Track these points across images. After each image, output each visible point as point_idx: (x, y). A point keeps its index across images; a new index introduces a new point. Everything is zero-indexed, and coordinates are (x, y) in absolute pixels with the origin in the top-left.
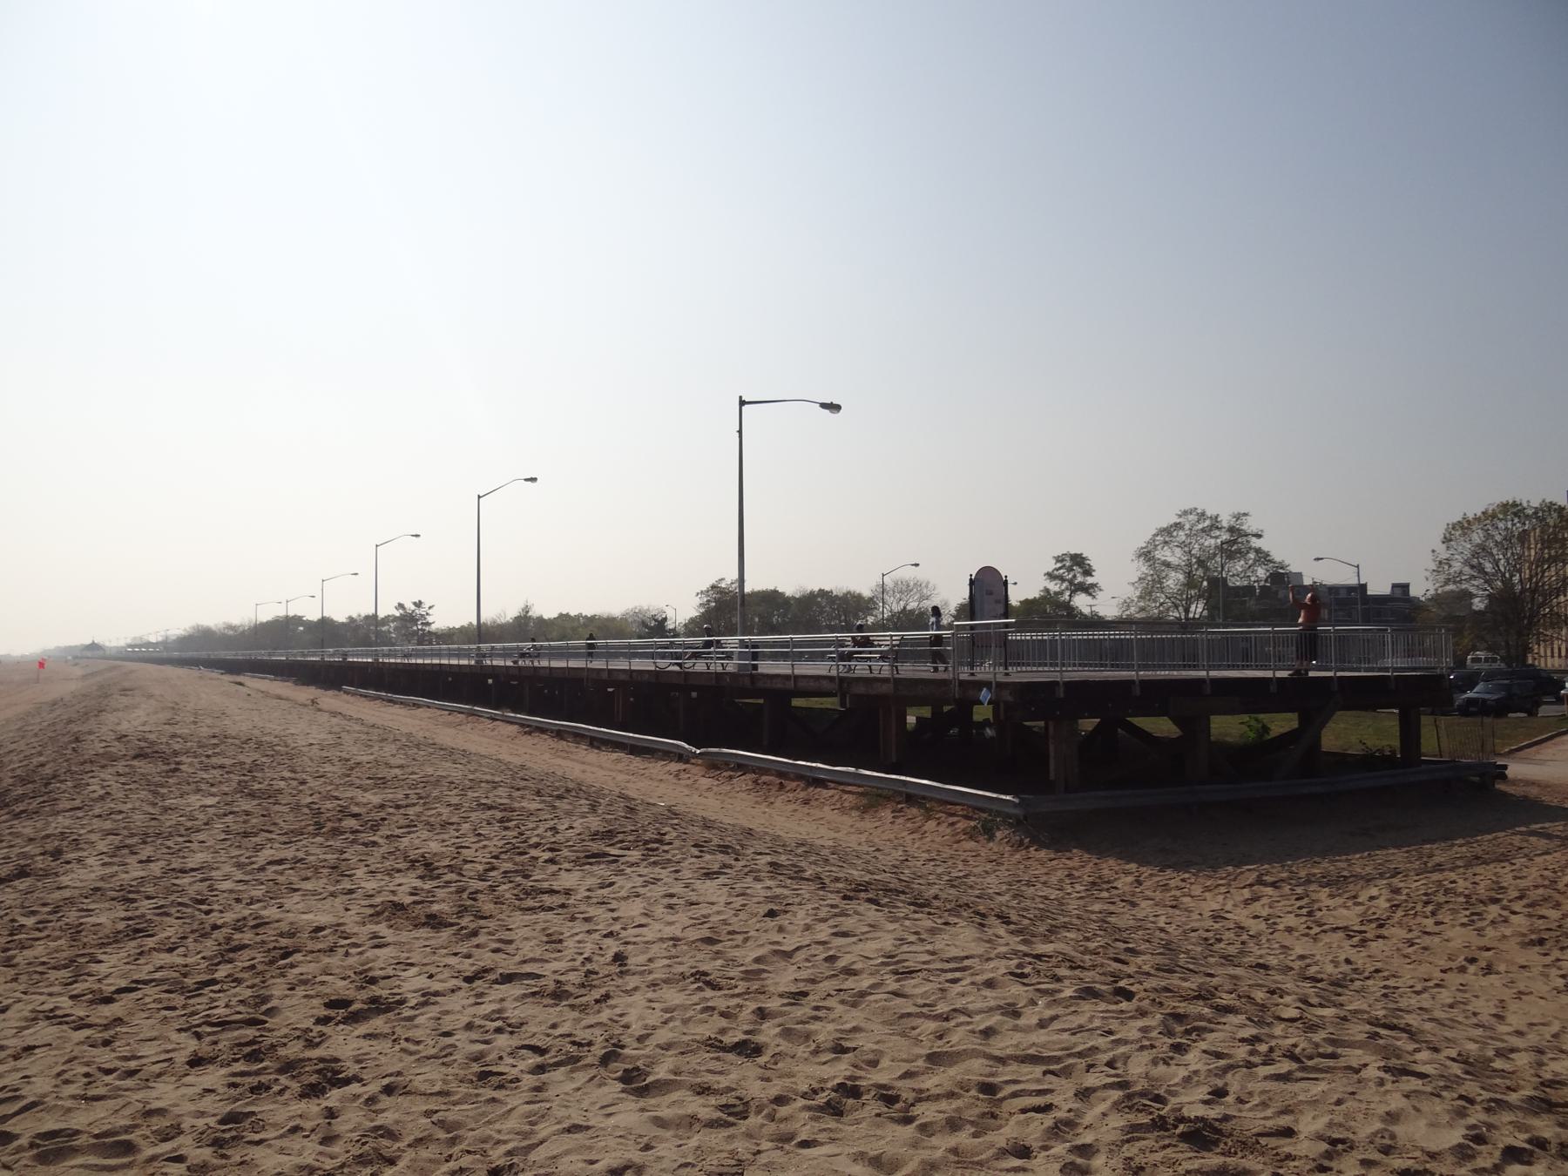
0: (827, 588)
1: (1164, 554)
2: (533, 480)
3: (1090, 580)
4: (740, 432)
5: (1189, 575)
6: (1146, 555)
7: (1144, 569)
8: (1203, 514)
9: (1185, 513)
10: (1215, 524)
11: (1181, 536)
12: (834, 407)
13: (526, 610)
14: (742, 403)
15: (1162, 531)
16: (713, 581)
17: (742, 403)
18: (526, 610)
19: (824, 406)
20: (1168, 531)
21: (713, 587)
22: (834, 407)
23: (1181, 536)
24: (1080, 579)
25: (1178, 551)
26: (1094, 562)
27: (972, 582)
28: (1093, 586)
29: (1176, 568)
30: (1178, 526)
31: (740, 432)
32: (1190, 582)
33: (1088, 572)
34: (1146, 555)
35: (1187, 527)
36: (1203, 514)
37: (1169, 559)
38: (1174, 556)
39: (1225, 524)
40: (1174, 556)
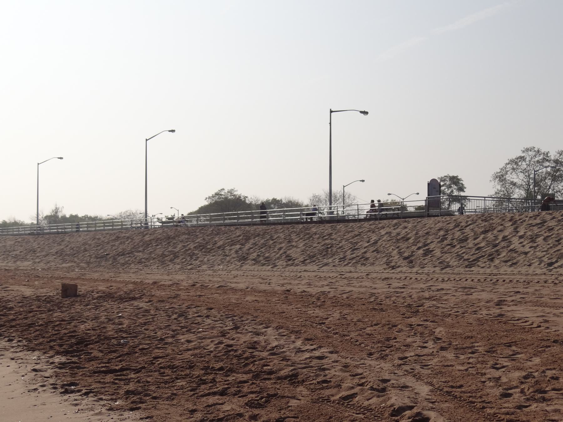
0: (278, 198)
1: (512, 177)
2: (173, 131)
3: (462, 194)
4: (330, 123)
5: (527, 191)
6: (501, 177)
7: (499, 187)
8: (538, 151)
9: (527, 150)
10: (546, 158)
11: (524, 165)
12: (365, 113)
13: (56, 211)
14: (331, 112)
15: (512, 162)
16: (216, 191)
17: (331, 112)
18: (56, 211)
19: (361, 112)
20: (515, 162)
21: (217, 194)
22: (365, 113)
23: (524, 165)
24: (456, 193)
25: (521, 176)
26: (465, 183)
27: (428, 184)
28: (465, 198)
29: (519, 187)
30: (522, 158)
31: (330, 123)
32: (530, 196)
33: (461, 189)
34: (501, 177)
35: (528, 159)
36: (538, 151)
37: (515, 181)
38: (518, 178)
39: (552, 158)
40: (518, 178)
